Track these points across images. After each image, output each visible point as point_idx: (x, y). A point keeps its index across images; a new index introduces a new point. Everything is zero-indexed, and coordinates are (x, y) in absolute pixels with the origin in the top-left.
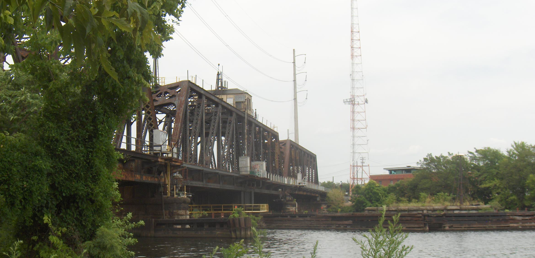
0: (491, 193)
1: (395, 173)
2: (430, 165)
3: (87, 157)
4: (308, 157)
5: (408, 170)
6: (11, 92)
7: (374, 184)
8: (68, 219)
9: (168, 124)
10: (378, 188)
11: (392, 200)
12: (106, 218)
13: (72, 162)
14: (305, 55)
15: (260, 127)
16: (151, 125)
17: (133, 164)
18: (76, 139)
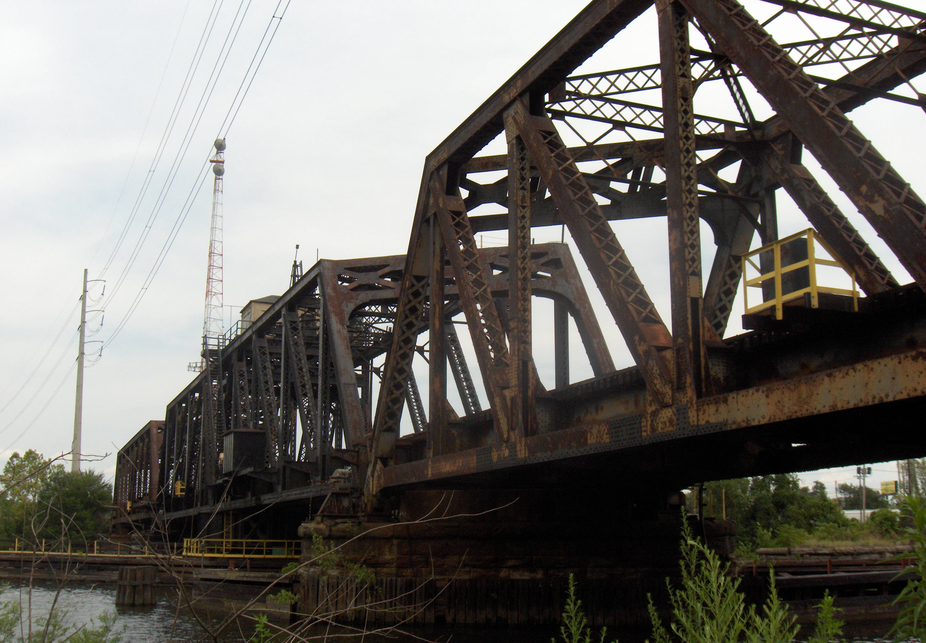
14: (105, 281)
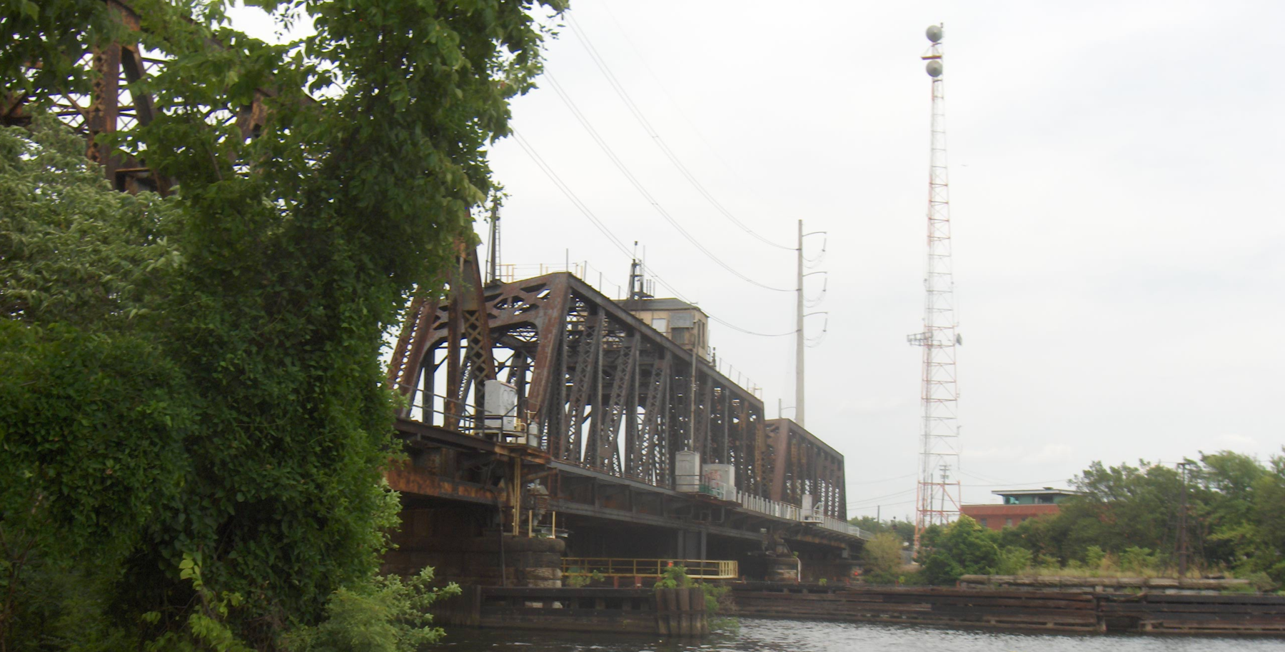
0: (1232, 553)
1: (1017, 502)
2: (1098, 485)
3: (307, 392)
4: (826, 459)
5: (1047, 497)
6: (131, 250)
7: (970, 525)
8: (251, 567)
9: (517, 371)
10: (980, 534)
11: (1022, 560)
12: (359, 571)
13: (264, 407)
14: (825, 233)
15: (723, 387)
16: (481, 369)
17: (437, 459)
18: (276, 342)
